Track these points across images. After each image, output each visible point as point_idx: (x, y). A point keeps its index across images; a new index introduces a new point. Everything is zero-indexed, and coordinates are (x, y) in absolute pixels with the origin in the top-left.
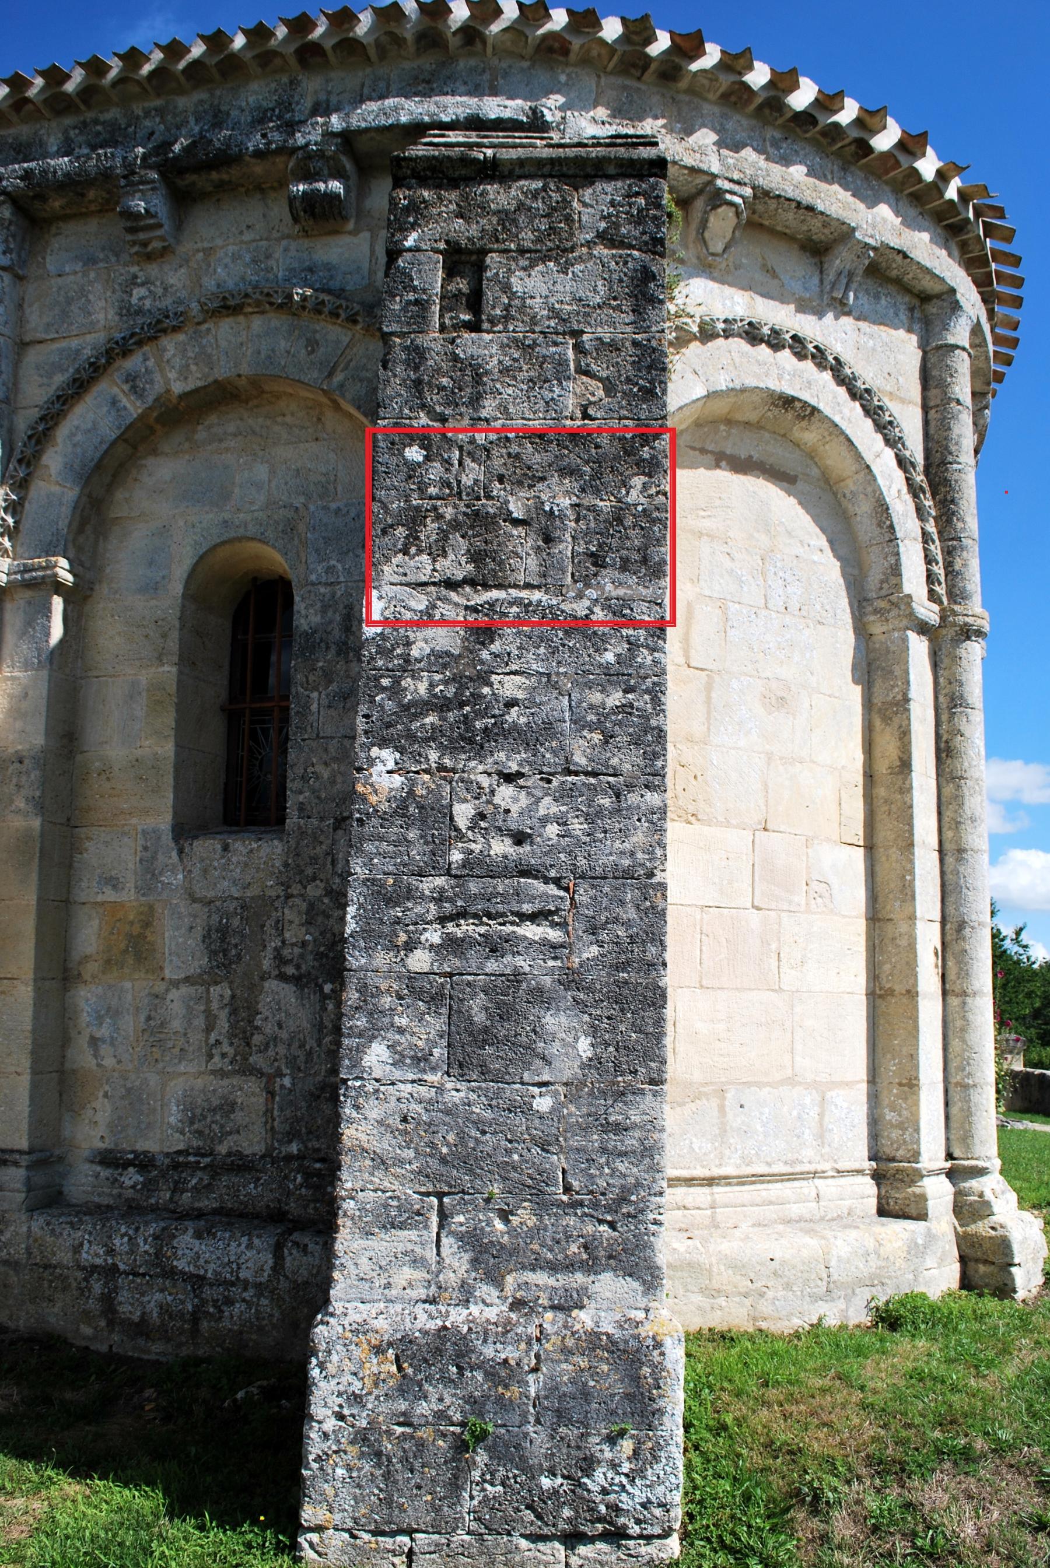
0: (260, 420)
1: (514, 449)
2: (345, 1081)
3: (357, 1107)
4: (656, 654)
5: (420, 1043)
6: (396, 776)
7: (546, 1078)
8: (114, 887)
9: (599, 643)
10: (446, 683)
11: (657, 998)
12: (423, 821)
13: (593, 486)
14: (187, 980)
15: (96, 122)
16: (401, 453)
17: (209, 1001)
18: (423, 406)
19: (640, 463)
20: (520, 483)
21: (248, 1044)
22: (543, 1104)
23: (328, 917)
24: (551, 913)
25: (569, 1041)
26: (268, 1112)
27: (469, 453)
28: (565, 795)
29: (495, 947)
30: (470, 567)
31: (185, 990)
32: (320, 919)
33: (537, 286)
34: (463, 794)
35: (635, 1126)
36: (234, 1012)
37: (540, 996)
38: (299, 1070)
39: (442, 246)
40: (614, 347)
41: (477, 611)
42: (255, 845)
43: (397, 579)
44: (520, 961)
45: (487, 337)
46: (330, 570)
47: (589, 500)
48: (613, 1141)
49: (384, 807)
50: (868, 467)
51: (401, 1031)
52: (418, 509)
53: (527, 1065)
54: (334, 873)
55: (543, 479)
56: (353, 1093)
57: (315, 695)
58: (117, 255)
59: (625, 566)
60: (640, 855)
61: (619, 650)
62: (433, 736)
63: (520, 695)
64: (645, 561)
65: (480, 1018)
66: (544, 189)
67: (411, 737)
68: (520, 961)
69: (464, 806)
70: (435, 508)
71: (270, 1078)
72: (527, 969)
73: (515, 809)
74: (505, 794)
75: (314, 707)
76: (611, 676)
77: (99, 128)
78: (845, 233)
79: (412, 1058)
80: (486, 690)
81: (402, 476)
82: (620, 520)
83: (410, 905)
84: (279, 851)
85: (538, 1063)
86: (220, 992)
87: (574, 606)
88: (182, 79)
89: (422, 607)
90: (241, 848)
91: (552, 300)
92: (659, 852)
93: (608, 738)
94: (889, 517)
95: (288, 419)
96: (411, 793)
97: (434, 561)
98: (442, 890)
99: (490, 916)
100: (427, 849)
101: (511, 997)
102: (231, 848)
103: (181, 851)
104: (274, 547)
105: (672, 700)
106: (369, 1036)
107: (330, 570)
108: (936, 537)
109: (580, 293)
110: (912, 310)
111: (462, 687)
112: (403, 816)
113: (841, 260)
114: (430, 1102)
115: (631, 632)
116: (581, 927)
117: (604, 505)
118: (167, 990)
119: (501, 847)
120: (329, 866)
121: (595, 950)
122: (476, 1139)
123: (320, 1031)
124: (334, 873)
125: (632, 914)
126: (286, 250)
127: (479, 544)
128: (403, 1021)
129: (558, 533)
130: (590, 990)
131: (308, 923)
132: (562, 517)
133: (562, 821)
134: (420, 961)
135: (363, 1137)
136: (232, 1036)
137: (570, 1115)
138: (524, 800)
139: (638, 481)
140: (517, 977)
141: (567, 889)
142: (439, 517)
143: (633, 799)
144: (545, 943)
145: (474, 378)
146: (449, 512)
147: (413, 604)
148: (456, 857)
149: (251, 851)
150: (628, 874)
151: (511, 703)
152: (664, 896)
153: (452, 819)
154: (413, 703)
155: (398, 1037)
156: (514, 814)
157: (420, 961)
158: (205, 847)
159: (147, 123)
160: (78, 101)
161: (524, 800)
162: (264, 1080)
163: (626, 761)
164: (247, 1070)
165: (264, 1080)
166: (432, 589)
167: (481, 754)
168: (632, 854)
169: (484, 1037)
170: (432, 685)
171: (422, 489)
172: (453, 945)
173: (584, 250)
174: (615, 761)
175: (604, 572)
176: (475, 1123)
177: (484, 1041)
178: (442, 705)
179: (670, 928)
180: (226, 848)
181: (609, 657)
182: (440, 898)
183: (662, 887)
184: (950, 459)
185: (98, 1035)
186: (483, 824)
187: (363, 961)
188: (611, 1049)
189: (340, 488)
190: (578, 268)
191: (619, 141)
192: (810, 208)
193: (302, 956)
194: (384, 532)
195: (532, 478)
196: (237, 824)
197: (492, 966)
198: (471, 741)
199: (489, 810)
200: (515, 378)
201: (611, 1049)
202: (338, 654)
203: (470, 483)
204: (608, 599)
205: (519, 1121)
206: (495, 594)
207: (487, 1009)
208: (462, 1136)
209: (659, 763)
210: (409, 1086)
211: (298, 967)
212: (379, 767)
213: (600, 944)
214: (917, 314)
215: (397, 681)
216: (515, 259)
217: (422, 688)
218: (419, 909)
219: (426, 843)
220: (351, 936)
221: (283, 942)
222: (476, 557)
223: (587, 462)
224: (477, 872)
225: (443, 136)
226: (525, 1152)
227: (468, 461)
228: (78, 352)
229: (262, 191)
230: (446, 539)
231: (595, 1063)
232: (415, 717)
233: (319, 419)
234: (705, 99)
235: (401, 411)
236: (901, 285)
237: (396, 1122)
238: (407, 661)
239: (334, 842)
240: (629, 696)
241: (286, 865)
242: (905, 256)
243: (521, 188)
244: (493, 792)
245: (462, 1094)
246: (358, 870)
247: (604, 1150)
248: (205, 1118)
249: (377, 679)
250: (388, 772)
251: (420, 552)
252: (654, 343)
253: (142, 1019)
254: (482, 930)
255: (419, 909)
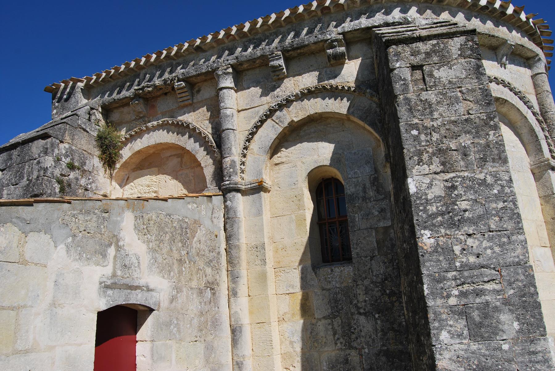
0: (322, 127)
1: (447, 127)
2: (434, 346)
3: (440, 354)
4: (511, 189)
5: (458, 330)
6: (431, 239)
7: (505, 338)
8: (293, 287)
9: (490, 186)
10: (442, 206)
11: (538, 306)
12: (444, 253)
13: (477, 135)
14: (324, 318)
15: (254, 39)
16: (410, 133)
17: (333, 325)
18: (414, 117)
19: (491, 126)
20: (452, 138)
21: (350, 338)
22: (505, 347)
23: (373, 291)
24: (494, 280)
25: (509, 324)
26: (361, 362)
27: (433, 130)
28: (490, 239)
29: (479, 293)
30: (442, 167)
31: (323, 321)
32: (370, 292)
33: (443, 74)
34: (456, 243)
35: (540, 352)
36: (343, 327)
37: (496, 309)
38: (371, 346)
39: (408, 65)
40: (473, 90)
41: (447, 181)
42: (342, 269)
43: (418, 174)
44: (488, 298)
45: (430, 92)
46: (355, 173)
47: (476, 140)
48: (533, 358)
49: (429, 250)
50: (526, 117)
51: (451, 326)
52: (419, 150)
53: (497, 334)
54: (373, 275)
55: (459, 136)
56: (438, 350)
57: (357, 215)
58: (267, 80)
59: (494, 160)
60: (521, 257)
61: (498, 189)
62: (441, 224)
63: (468, 207)
64: (500, 158)
65: (477, 319)
66: (438, 43)
67: (434, 225)
68: (488, 298)
69: (457, 247)
70: (425, 149)
71: (360, 350)
72: (490, 300)
73: (474, 246)
74: (470, 241)
75: (357, 219)
76: (497, 198)
77: (255, 41)
78: (504, 42)
79: (457, 335)
80: (456, 207)
81: (412, 140)
82: (489, 146)
83: (445, 282)
84: (352, 269)
85: (501, 333)
86: (337, 322)
87: (479, 176)
88: (283, 23)
89: (428, 182)
90: (338, 270)
91: (449, 78)
92: (527, 255)
93: (501, 219)
94: (535, 133)
95: (332, 125)
96: (438, 244)
97: (429, 166)
98: (455, 276)
99: (474, 283)
100: (448, 262)
101: (487, 311)
102: (334, 270)
103: (315, 273)
104: (334, 167)
105: (520, 204)
106: (440, 329)
107: (355, 173)
108: (549, 137)
109: (458, 75)
110: (524, 63)
111: (448, 207)
112: (437, 252)
113: (503, 50)
114: (466, 350)
115: (501, 182)
116: (506, 284)
117: (482, 142)
118: (317, 322)
119: (472, 259)
120: (371, 273)
121: (512, 292)
122: (485, 362)
123: (376, 331)
124: (373, 275)
125: (522, 277)
126: (326, 72)
127: (443, 159)
128: (451, 323)
129: (469, 153)
130: (513, 305)
131: (366, 294)
132: (469, 147)
133: (491, 248)
134: (453, 301)
135: (444, 364)
136: (343, 336)
137: (516, 350)
138: (477, 243)
139: (491, 133)
140: (487, 303)
141: (498, 271)
142: (428, 152)
143: (514, 238)
144: (494, 290)
145: (428, 106)
146: (430, 150)
147: (425, 181)
148: (458, 264)
149: (341, 271)
150: (518, 264)
151: (465, 211)
152: (533, 270)
153: (453, 251)
154: (433, 214)
155: (450, 328)
156: (475, 248)
157: (453, 301)
158: (325, 271)
159: (272, 37)
160: (248, 33)
161: (477, 243)
162: (358, 351)
163: (509, 225)
164: (351, 347)
165: (358, 351)
166: (430, 175)
167: (458, 228)
168: (518, 257)
169: (480, 325)
170: (437, 207)
171: (420, 144)
172: (463, 294)
173: (456, 61)
174: (505, 226)
175: (487, 164)
176: (483, 356)
177: (482, 328)
178: (442, 214)
179: (536, 281)
180: (332, 271)
181: (495, 191)
182: (455, 279)
183: (531, 267)
184: (548, 110)
185: (293, 340)
186: (465, 252)
187: (433, 303)
188: (525, 325)
189: (354, 146)
190: (455, 67)
191: (438, 25)
192: (493, 36)
193: (365, 305)
194: (410, 159)
195: (456, 136)
196: (329, 262)
197: (478, 300)
198: (455, 224)
199: (466, 247)
200: (442, 104)
201: (525, 325)
202: (363, 201)
203: (435, 140)
204: (490, 172)
205: (498, 353)
206: (452, 175)
207: (479, 316)
208: (479, 361)
209: (520, 225)
210: (458, 345)
211: (365, 310)
212: (425, 237)
213: (513, 289)
214: (527, 65)
215: (425, 208)
216: (433, 66)
217: (434, 209)
218: (448, 283)
219: (447, 260)
220: (427, 295)
221: (358, 301)
222: (443, 164)
223: (473, 128)
224: (466, 269)
225: (380, 30)
226: (503, 365)
227: (433, 133)
228: (258, 112)
229: (314, 54)
230: (431, 159)
231: (520, 331)
232: (434, 218)
233: (343, 124)
234: (452, 7)
235: (407, 119)
236: (520, 56)
237: (455, 358)
238: (427, 200)
239: (371, 265)
240: (506, 203)
241: (355, 274)
242: (523, 46)
243: (430, 44)
244: (466, 241)
245: (477, 346)
246: (425, 272)
247: (530, 361)
248: (337, 366)
249: (418, 207)
250: (429, 238)
251: (423, 164)
252: (486, 88)
253: (309, 333)
254: (472, 288)
255: (448, 283)
